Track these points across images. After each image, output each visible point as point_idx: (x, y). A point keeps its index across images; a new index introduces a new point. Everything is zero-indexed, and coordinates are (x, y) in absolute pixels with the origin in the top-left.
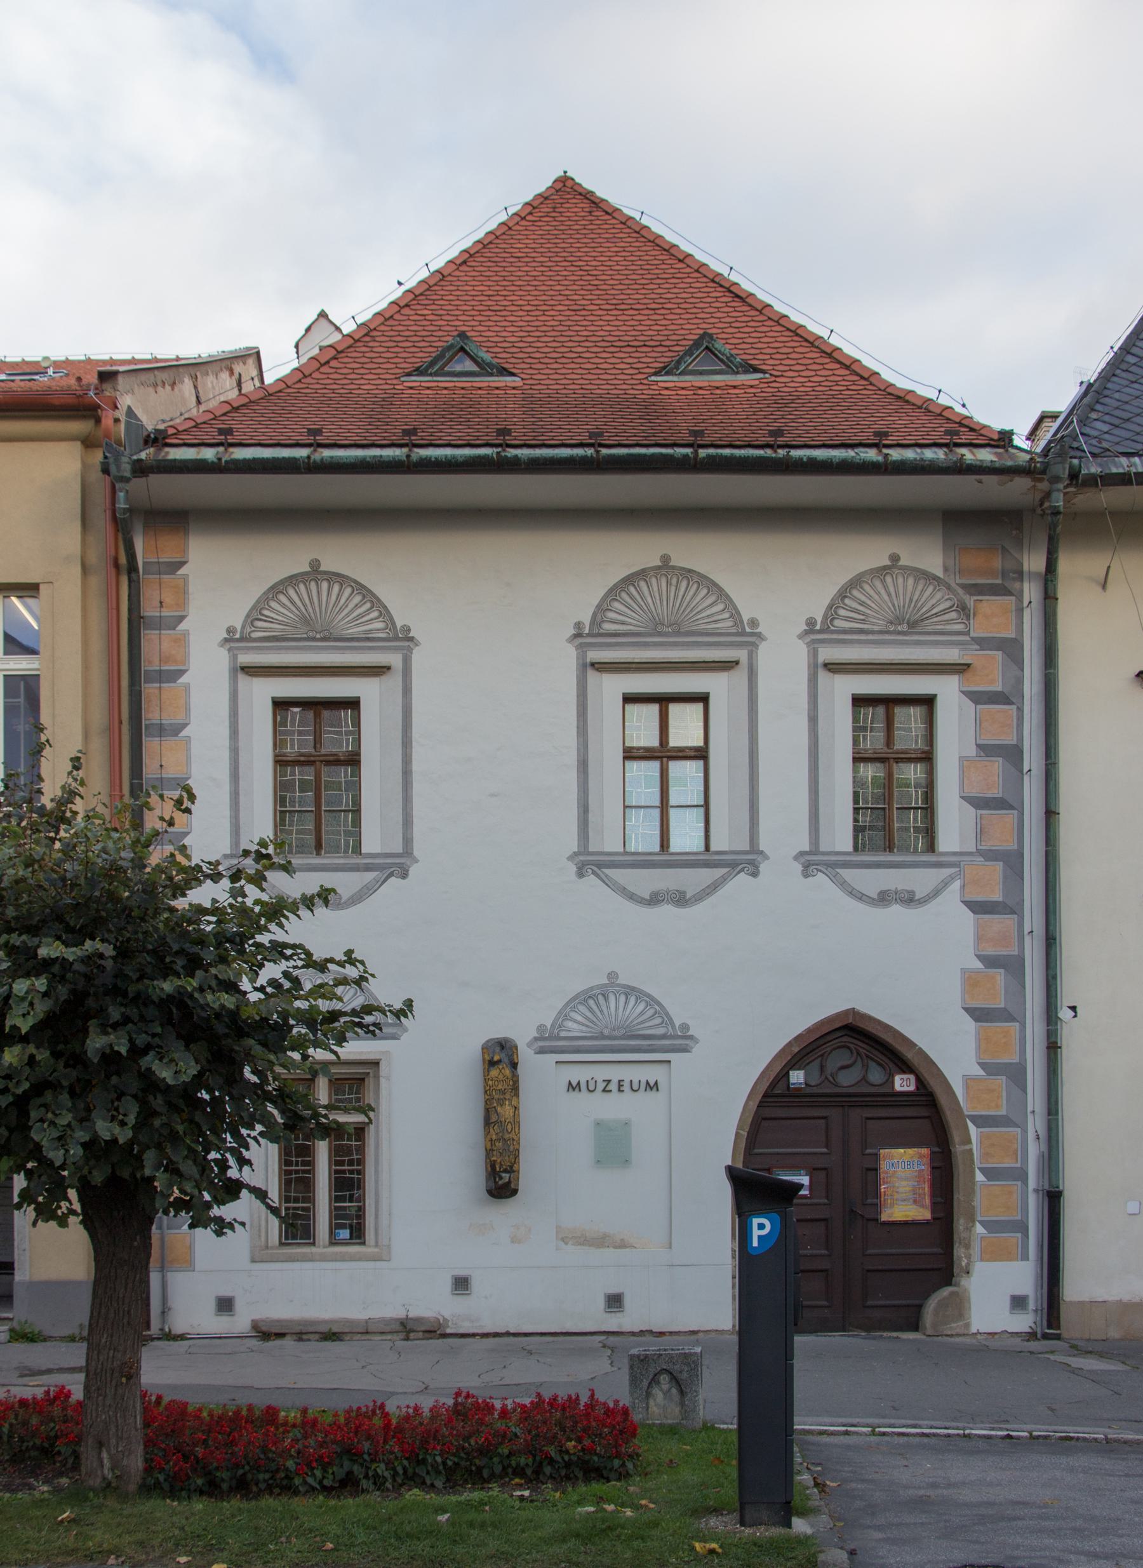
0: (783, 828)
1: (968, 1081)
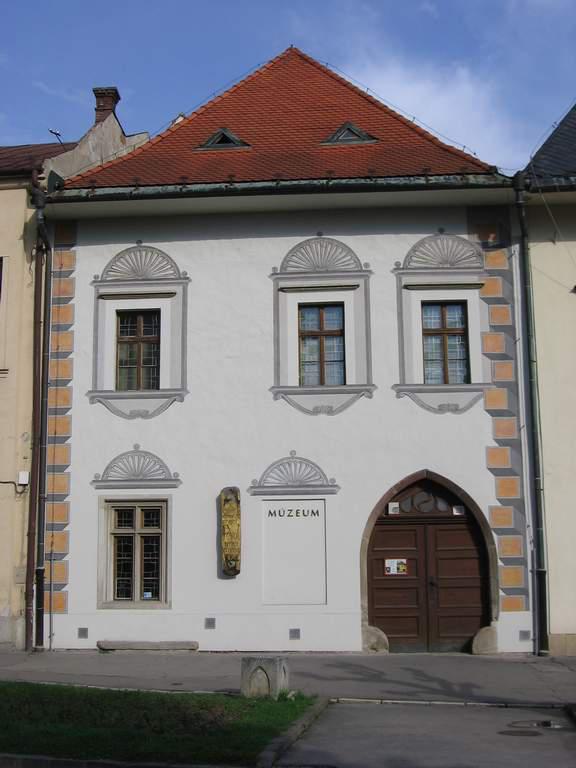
0: (385, 374)
1: (491, 509)
